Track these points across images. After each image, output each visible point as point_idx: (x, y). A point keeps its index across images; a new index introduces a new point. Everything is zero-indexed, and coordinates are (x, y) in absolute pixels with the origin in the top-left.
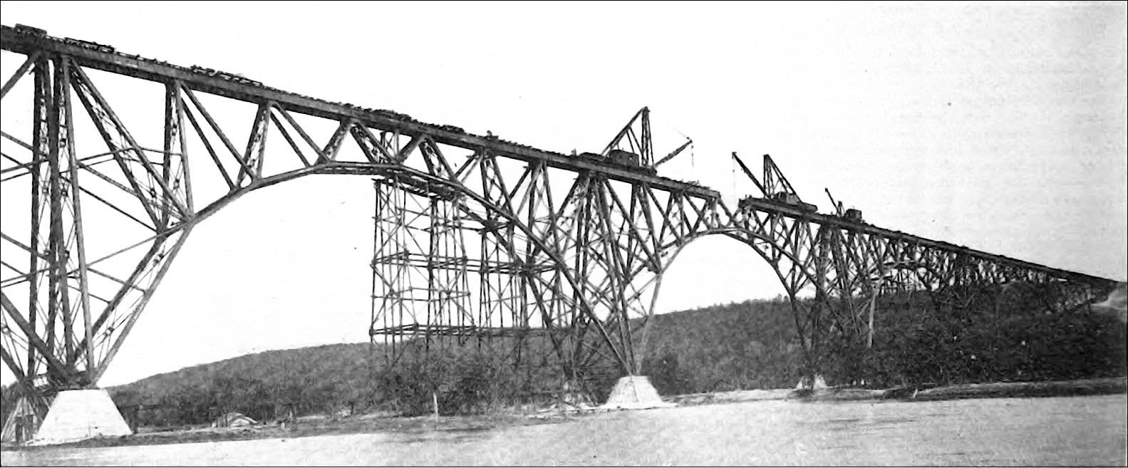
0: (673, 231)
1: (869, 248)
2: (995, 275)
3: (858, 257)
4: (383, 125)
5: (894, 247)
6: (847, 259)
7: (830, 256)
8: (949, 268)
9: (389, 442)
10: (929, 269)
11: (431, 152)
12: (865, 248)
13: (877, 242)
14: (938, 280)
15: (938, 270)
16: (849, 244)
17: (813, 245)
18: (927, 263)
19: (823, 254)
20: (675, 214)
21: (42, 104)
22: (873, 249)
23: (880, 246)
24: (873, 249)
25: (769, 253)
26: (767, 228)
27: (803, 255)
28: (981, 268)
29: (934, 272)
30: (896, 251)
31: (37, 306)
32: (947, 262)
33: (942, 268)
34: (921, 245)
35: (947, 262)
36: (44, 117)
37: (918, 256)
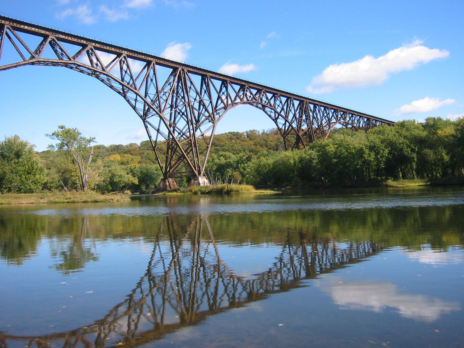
0: (222, 102)
1: (323, 114)
3: (318, 119)
5: (336, 114)
12: (322, 114)
13: (327, 111)
17: (295, 111)
18: (352, 123)
20: (171, 83)
22: (325, 115)
25: (273, 115)
30: (337, 116)
35: (361, 123)
37: (348, 119)
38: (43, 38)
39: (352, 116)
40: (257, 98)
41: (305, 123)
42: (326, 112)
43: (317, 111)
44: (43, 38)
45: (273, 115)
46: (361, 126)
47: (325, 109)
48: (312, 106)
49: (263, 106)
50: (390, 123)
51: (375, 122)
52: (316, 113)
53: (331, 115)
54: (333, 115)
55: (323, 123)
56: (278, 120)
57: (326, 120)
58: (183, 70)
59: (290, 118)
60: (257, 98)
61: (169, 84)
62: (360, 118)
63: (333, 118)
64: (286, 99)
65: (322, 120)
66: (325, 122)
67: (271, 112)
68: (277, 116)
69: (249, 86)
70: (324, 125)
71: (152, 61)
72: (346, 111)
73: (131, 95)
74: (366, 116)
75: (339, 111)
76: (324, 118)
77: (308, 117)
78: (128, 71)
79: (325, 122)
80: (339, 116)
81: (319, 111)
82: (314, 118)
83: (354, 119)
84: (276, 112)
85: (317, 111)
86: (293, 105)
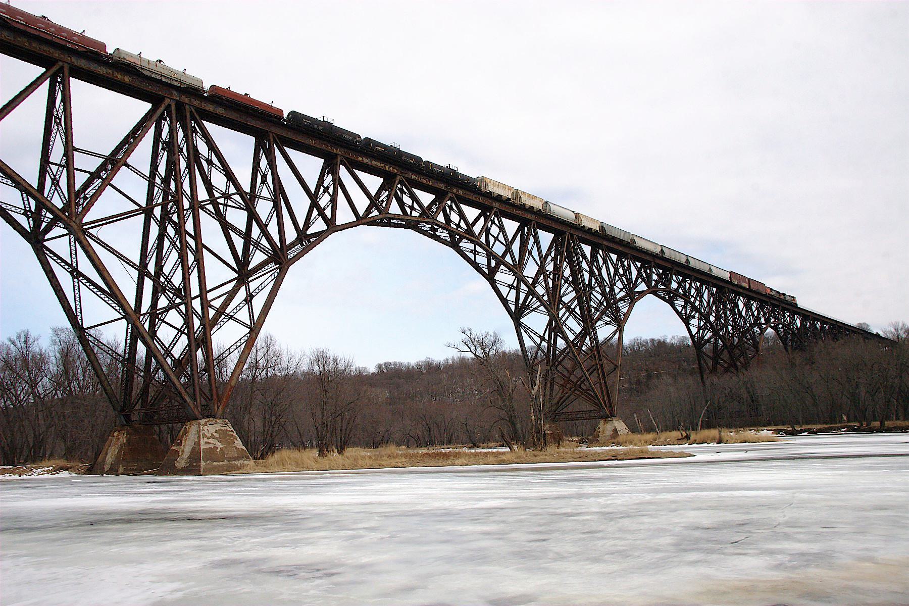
0: (321, 213)
1: (616, 270)
2: (756, 313)
3: (603, 279)
4: (447, 179)
5: (646, 272)
6: (590, 280)
7: (567, 272)
8: (708, 303)
9: (574, 546)
10: (687, 301)
11: (196, 132)
12: (612, 270)
13: (626, 263)
14: (697, 315)
15: (697, 303)
16: (592, 262)
17: (543, 259)
18: (685, 294)
19: (558, 269)
20: (328, 188)
21: (101, 177)
22: (621, 271)
23: (629, 268)
24: (621, 271)
25: (482, 260)
26: (477, 229)
27: (531, 270)
28: (741, 305)
29: (693, 304)
30: (649, 277)
31: (741, 556)
32: (706, 296)
33: (701, 301)
34: (678, 274)
35: (706, 296)
36: (529, 311)
37: (674, 285)
38: (151, 105)
39: (684, 281)
40: (383, 201)
41: (570, 289)
42: (623, 265)
43: (601, 261)
44: (151, 105)
45: (482, 260)
46: (596, 306)
47: (619, 260)
48: (587, 249)
49: (452, 234)
50: (83, 218)
51: (735, 297)
52: (598, 263)
53: (634, 273)
54: (639, 275)
55: (617, 290)
56: (498, 277)
57: (622, 282)
58: (571, 235)
59: (531, 270)
60: (383, 201)
61: (324, 192)
62: (701, 286)
63: (640, 280)
64: (517, 225)
65: (612, 285)
66: (622, 287)
67: (475, 252)
68: (493, 263)
69: (405, 178)
70: (618, 297)
71: (531, 221)
72: (777, 303)
73: (466, 245)
74: (715, 281)
75: (653, 264)
76: (617, 278)
77: (576, 271)
78: (416, 206)
79: (622, 287)
80: (655, 277)
81: (605, 262)
82: (591, 273)
83: (688, 286)
84: (490, 255)
85: (601, 261)
86: (537, 241)
